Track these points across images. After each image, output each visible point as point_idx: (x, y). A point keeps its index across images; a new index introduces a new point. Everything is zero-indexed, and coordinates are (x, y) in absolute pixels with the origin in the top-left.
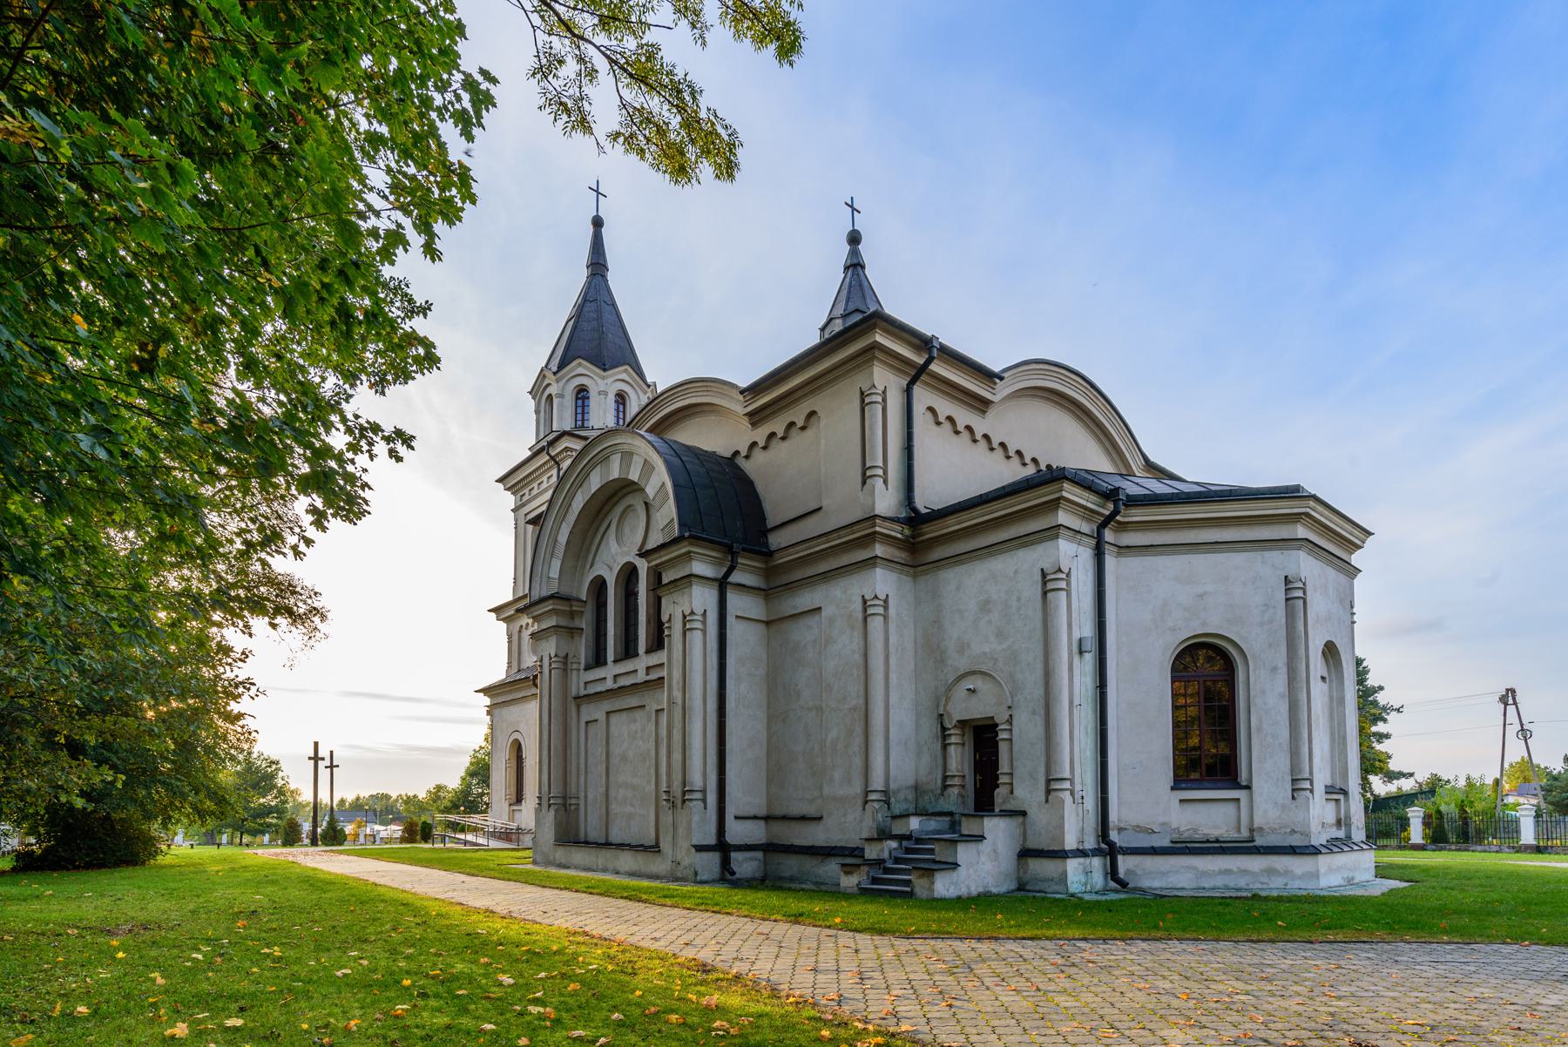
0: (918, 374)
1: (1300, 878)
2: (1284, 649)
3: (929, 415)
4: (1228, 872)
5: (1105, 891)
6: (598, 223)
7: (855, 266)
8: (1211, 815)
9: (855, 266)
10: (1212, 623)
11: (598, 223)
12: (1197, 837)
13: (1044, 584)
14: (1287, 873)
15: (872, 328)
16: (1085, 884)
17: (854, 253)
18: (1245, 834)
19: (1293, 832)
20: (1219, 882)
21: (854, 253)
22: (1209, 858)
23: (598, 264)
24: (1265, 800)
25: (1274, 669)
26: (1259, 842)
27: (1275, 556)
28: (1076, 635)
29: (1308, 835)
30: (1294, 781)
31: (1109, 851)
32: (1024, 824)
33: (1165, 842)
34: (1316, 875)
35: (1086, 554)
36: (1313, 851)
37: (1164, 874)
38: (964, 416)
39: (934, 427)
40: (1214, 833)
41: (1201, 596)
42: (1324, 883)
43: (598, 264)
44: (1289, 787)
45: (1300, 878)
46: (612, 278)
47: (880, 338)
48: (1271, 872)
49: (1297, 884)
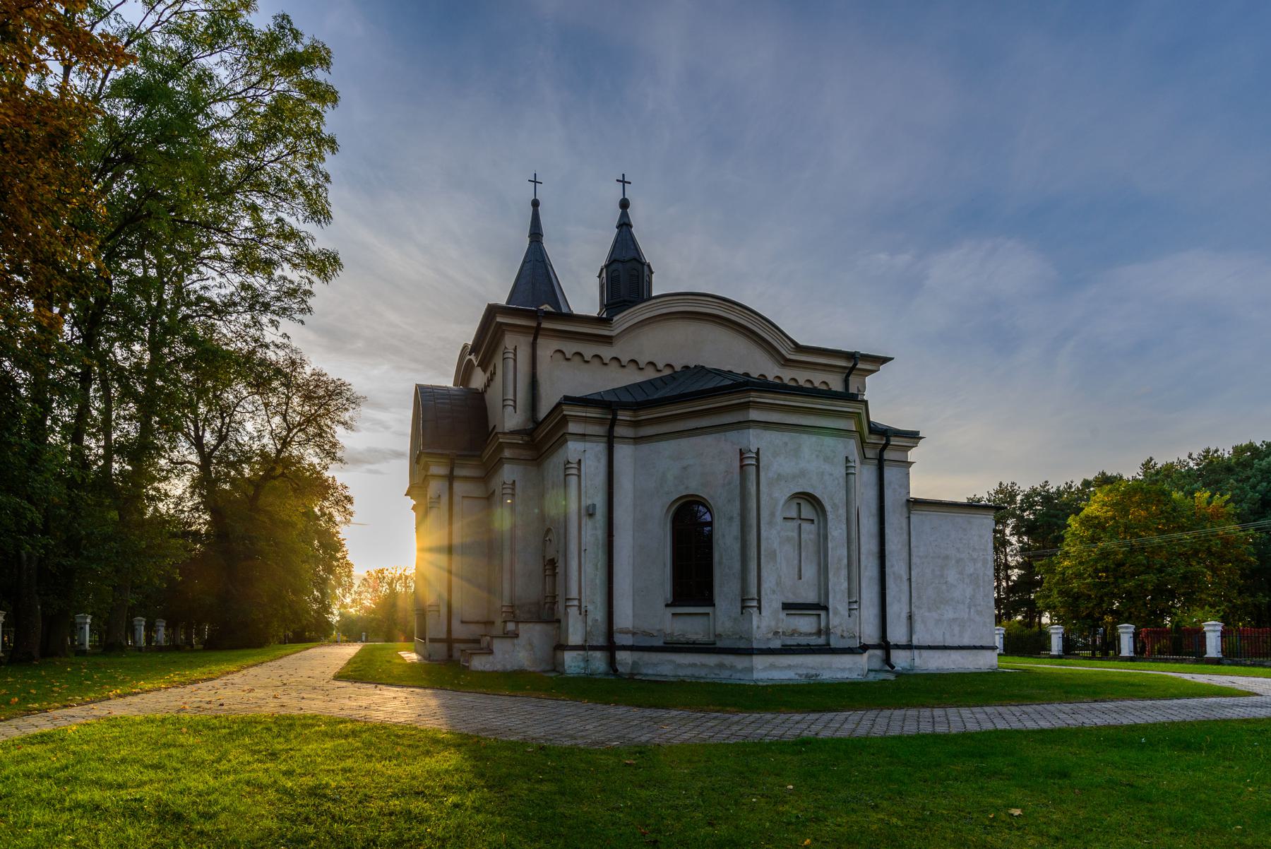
0: (537, 332)
1: (741, 671)
2: (738, 503)
3: (559, 355)
4: (694, 665)
5: (607, 674)
6: (535, 204)
7: (624, 225)
8: (691, 626)
9: (624, 225)
10: (693, 487)
11: (535, 204)
12: (683, 640)
13: (741, 460)
14: (732, 667)
15: (494, 317)
16: (585, 669)
17: (624, 215)
18: (712, 639)
19: (741, 638)
20: (689, 672)
21: (624, 215)
22: (683, 655)
23: (536, 234)
24: (723, 616)
25: (731, 519)
26: (719, 644)
27: (733, 435)
28: (586, 502)
29: (750, 640)
30: (743, 600)
31: (611, 648)
32: (559, 628)
33: (660, 643)
34: (750, 670)
35: (599, 448)
36: (750, 652)
37: (655, 665)
38: (589, 350)
39: (565, 363)
40: (693, 637)
41: (685, 468)
42: (756, 675)
43: (536, 234)
44: (739, 605)
45: (741, 671)
46: (547, 245)
47: (499, 319)
48: (721, 666)
49: (738, 675)
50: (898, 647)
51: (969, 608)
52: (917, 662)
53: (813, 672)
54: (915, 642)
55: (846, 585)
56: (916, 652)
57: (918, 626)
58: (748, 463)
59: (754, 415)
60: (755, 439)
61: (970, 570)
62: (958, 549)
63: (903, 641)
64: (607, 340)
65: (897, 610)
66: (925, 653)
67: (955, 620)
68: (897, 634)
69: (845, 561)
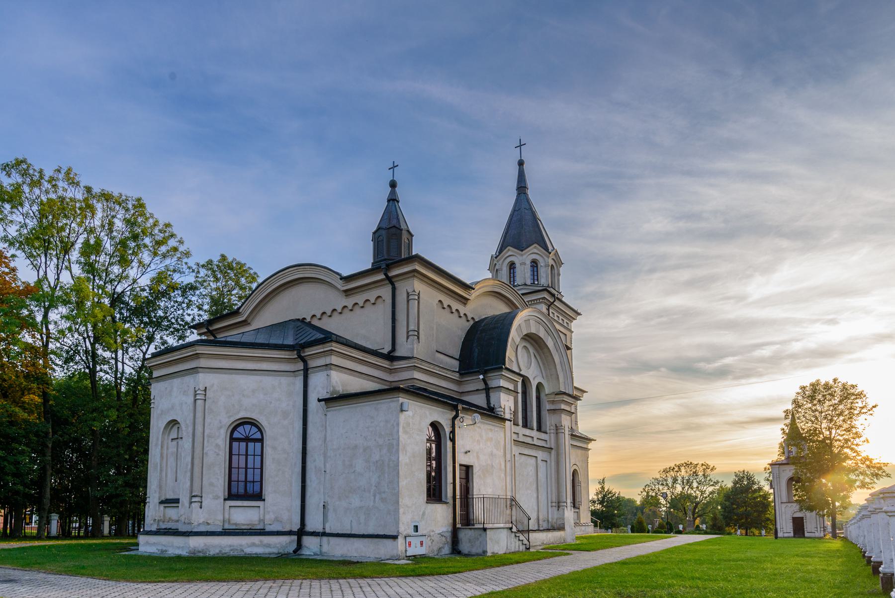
7: (393, 200)
8: (244, 514)
27: (189, 380)
50: (314, 534)
51: (375, 496)
52: (325, 548)
53: (164, 549)
54: (328, 531)
55: (189, 484)
56: (325, 539)
57: (331, 515)
58: (200, 396)
59: (203, 362)
60: (204, 379)
61: (376, 457)
62: (365, 438)
63: (536, 528)
64: (245, 323)
65: (313, 501)
66: (333, 540)
67: (361, 508)
68: (313, 524)
69: (189, 466)
